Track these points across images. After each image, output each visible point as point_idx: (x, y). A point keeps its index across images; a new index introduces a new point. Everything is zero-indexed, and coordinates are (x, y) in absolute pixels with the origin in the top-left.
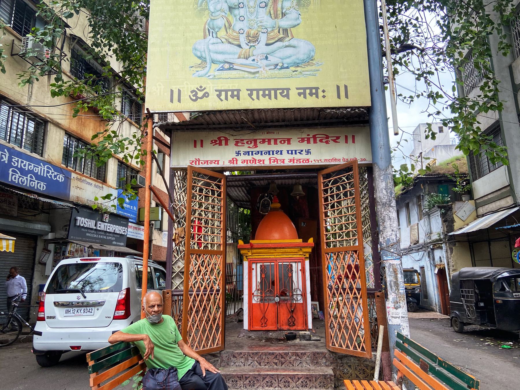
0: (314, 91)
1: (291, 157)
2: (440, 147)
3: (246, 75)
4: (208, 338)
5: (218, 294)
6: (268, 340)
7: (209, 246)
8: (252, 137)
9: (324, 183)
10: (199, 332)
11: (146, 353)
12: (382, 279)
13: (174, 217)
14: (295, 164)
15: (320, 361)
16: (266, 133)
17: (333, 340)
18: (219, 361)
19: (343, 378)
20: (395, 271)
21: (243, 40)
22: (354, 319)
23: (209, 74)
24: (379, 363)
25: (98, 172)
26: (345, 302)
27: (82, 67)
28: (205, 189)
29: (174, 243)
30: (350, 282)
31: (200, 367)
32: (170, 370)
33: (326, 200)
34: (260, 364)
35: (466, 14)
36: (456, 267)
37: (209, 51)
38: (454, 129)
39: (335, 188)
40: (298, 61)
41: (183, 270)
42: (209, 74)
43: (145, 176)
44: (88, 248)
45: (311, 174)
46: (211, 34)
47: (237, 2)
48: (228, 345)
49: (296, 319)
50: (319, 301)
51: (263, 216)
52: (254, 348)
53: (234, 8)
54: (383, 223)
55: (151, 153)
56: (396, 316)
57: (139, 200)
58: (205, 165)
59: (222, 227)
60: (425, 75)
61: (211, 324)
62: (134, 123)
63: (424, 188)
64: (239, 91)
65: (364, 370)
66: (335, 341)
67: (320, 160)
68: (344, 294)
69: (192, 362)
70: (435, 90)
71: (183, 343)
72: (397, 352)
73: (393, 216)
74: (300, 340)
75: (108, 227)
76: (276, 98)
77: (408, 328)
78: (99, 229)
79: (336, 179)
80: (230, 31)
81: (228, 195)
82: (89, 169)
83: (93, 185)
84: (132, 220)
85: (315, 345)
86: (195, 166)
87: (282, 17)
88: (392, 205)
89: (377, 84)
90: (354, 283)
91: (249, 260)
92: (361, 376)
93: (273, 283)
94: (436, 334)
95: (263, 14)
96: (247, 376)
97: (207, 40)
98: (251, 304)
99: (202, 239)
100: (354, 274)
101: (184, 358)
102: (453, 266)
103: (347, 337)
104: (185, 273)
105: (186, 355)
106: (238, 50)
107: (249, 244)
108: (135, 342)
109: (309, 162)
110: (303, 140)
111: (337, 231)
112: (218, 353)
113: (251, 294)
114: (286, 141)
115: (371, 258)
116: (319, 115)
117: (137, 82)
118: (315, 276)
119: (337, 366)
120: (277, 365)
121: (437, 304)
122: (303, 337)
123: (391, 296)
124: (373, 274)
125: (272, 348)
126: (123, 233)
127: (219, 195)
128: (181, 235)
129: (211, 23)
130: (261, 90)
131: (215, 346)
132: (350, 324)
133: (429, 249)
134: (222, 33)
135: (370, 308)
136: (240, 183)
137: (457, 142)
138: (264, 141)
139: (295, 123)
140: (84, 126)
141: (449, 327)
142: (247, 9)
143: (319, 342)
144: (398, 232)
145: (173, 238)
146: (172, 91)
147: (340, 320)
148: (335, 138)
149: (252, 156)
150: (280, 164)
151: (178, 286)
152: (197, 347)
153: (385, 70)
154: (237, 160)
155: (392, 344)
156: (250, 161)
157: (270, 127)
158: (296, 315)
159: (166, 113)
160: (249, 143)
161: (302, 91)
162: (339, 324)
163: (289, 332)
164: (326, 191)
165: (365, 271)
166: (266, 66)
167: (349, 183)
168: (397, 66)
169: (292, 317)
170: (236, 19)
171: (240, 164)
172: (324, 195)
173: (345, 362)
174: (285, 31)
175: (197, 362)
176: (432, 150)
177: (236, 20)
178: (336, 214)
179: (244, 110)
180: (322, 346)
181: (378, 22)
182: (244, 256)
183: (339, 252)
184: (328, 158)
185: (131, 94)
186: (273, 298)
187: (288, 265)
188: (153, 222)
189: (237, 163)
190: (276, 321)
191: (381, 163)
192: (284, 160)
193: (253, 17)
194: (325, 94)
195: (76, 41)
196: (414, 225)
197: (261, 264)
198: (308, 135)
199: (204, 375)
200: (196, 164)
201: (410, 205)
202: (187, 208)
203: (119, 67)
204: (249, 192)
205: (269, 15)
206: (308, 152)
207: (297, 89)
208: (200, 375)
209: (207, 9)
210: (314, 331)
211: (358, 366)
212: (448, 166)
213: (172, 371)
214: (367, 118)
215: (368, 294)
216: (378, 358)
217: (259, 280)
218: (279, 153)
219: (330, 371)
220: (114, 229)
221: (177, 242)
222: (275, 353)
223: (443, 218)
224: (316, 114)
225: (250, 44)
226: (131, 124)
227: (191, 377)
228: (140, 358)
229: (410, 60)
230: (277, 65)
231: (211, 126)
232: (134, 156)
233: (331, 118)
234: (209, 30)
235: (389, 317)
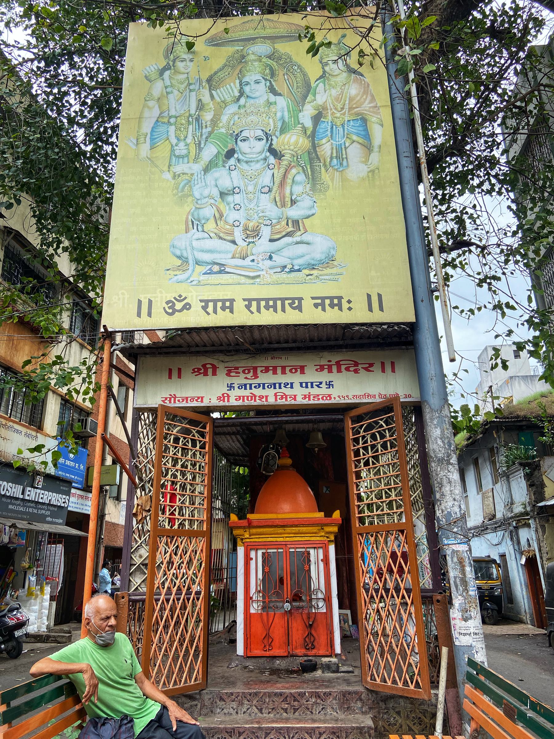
0: (336, 301)
1: (306, 391)
2: (517, 378)
3: (243, 280)
4: (181, 670)
5: (198, 599)
6: (275, 672)
7: (187, 523)
8: (250, 363)
9: (353, 428)
10: (168, 659)
11: (86, 693)
12: (444, 574)
13: (137, 480)
14: (312, 402)
15: (352, 705)
16: (269, 358)
17: (372, 671)
18: (199, 706)
19: (388, 731)
20: (461, 562)
21: (238, 235)
22: (403, 637)
23: (191, 279)
24: (443, 707)
25: (31, 415)
26: (388, 610)
27: (18, 270)
28: (182, 439)
29: (134, 519)
30: (396, 579)
31: (169, 716)
32: (122, 720)
33: (357, 453)
34: (261, 710)
35: (542, 199)
36: (552, 553)
37: (193, 248)
38: (532, 354)
39: (369, 436)
40: (313, 262)
41: (147, 562)
42: (191, 279)
43: (97, 420)
44: (10, 527)
45: (334, 417)
46: (195, 227)
47: (232, 186)
48: (212, 680)
49: (316, 637)
50: (350, 609)
51: (267, 477)
52: (252, 685)
53: (227, 194)
54: (440, 489)
55: (107, 387)
56: (465, 632)
57: (88, 455)
58: (184, 404)
59: (206, 495)
60: (488, 281)
61: (187, 647)
62: (86, 345)
63: (499, 437)
64: (232, 301)
65: (420, 718)
66: (375, 673)
67: (347, 396)
68: (388, 598)
69: (156, 708)
70: (504, 299)
71: (143, 677)
72: (468, 688)
73: (454, 477)
74: (323, 672)
75: (41, 496)
76: (283, 310)
77: (484, 650)
78: (27, 498)
79: (370, 423)
80: (221, 224)
81: (215, 445)
82: (19, 411)
83: (23, 433)
84: (76, 485)
85: (345, 680)
86: (170, 405)
87: (292, 205)
88: (451, 461)
89: (422, 292)
90: (402, 581)
91: (246, 544)
92: (416, 728)
93: (281, 581)
94: (528, 659)
95: (265, 201)
96: (241, 730)
97: (189, 235)
98: (248, 614)
99: (177, 513)
100: (400, 566)
101: (144, 702)
102: (547, 553)
103: (393, 667)
104: (149, 567)
105: (147, 696)
106: (232, 247)
107: (246, 521)
108: (70, 675)
109: (331, 398)
110: (322, 368)
111: (375, 500)
112: (196, 694)
113: (249, 598)
114: (299, 370)
115: (425, 541)
116: (344, 333)
117: (94, 289)
118: (344, 569)
119: (379, 713)
120: (287, 713)
121: (527, 611)
122: (328, 667)
123: (457, 601)
124: (429, 566)
125: (279, 685)
126: (63, 505)
127: (203, 447)
128: (145, 506)
129: (196, 214)
130: (263, 299)
131: (192, 683)
132: (397, 646)
133: (511, 528)
134: (210, 226)
135: (427, 620)
136: (234, 429)
137: (541, 370)
138: (267, 370)
139: (311, 344)
140: (16, 350)
141: (546, 647)
142: (245, 195)
143: (351, 674)
144: (462, 502)
145: (134, 511)
146: (140, 302)
147: (382, 639)
148: (368, 365)
149: (251, 391)
150: (290, 401)
151: (139, 585)
152: (164, 683)
153: (432, 274)
154: (228, 396)
155: (460, 677)
156: (248, 397)
157: (275, 350)
158: (316, 631)
159: (133, 331)
160: (247, 371)
161: (319, 301)
162: (381, 645)
163: (306, 658)
164: (356, 441)
165: (416, 562)
166: (271, 268)
167: (390, 430)
168: (449, 270)
169: (310, 634)
170: (230, 207)
171: (233, 402)
172: (354, 446)
173: (391, 705)
174: (296, 223)
175: (164, 708)
176: (506, 382)
177: (230, 209)
178: (372, 475)
179: (239, 327)
180: (356, 682)
181: (421, 212)
182: (238, 539)
183: (378, 532)
184: (358, 393)
185: (84, 306)
186: (281, 604)
187: (303, 553)
188: (108, 487)
189: (228, 401)
190: (287, 642)
191: (433, 401)
192: (295, 396)
193: (252, 206)
194: (351, 305)
195: (12, 236)
196: (487, 492)
197: (264, 551)
198: (330, 361)
199: (174, 729)
200: (170, 402)
201: (480, 462)
202: (156, 466)
203: (70, 270)
204: (246, 443)
205: (274, 203)
206: (330, 385)
207: (313, 298)
208: (168, 729)
209: (190, 195)
210: (344, 658)
211: (411, 712)
212: (530, 406)
213: (125, 722)
214: (410, 338)
215: (423, 597)
216: (441, 698)
217: (260, 576)
218: (289, 386)
219: (368, 722)
220: (49, 498)
221: (140, 518)
222: (285, 693)
223: (528, 481)
224: (339, 332)
225: (248, 240)
226: (82, 346)
227: (153, 732)
228: (78, 700)
229: (467, 261)
230: (285, 267)
231: (193, 349)
232: (82, 391)
233: (361, 338)
234: (193, 222)
235: (455, 634)
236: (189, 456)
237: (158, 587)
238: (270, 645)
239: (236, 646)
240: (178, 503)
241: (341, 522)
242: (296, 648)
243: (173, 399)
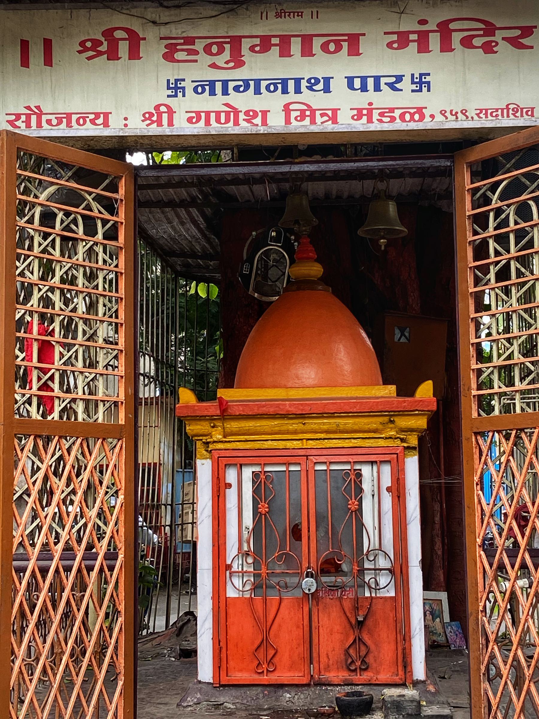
5: (111, 569)
7: (80, 408)
9: (474, 191)
14: (375, 126)
16: (272, 14)
28: (60, 216)
39: (512, 211)
45: (428, 163)
49: (372, 647)
58: (62, 131)
59: (121, 345)
61: (90, 665)
67: (464, 112)
79: (516, 179)
91: (216, 455)
99: (56, 386)
109: (422, 117)
113: (223, 568)
114: (345, 45)
118: (437, 507)
127: (113, 284)
136: (183, 193)
147: (519, 652)
148: (518, 32)
154: (171, 112)
156: (218, 114)
158: (370, 632)
160: (215, 49)
162: (516, 666)
163: (348, 689)
169: (359, 641)
172: (475, 233)
178: (514, 300)
182: (199, 444)
183: (522, 430)
186: (296, 580)
187: (347, 474)
189: (171, 123)
190: (307, 655)
192: (335, 111)
197: (257, 469)
198: (423, 22)
200: (28, 126)
210: (432, 688)
217: (248, 521)
218: (320, 86)
236: (80, 256)
237: (21, 544)
238: (270, 662)
239: (196, 662)
240: (58, 363)
241: (434, 407)
242: (328, 668)
243: (34, 118)
